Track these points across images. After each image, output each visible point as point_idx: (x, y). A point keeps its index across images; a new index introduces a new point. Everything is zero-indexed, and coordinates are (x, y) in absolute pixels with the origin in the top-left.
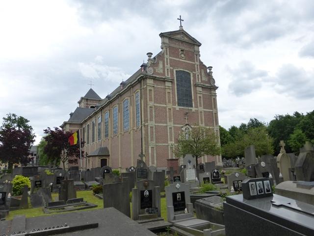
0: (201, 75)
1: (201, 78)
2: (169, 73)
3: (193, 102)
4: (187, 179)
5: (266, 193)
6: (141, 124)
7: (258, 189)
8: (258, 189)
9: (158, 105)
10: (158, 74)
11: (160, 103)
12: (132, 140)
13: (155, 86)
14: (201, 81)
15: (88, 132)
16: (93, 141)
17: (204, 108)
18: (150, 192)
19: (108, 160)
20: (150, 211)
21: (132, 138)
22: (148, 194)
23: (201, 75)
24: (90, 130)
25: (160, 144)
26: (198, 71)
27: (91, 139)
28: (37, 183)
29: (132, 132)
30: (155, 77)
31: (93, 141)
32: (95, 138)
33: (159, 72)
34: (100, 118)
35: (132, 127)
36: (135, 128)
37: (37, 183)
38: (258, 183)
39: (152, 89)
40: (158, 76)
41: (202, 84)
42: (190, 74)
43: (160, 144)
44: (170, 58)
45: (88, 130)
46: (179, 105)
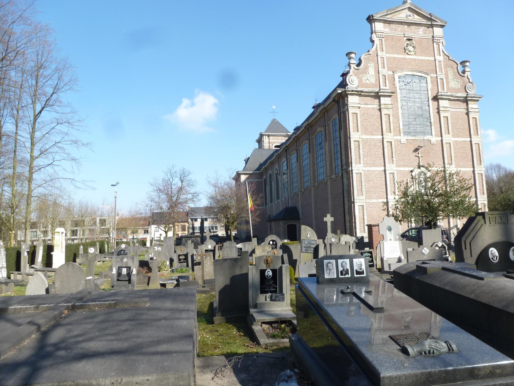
0: (447, 78)
1: (448, 84)
2: (387, 81)
4: (319, 257)
5: (355, 276)
6: (342, 170)
7: (340, 269)
8: (340, 269)
9: (369, 137)
10: (367, 86)
11: (372, 134)
12: (329, 195)
13: (362, 106)
14: (448, 89)
15: (271, 186)
16: (271, 201)
17: (454, 136)
18: (274, 271)
19: (297, 226)
20: (273, 298)
21: (329, 192)
22: (271, 274)
23: (447, 78)
24: (267, 187)
25: (373, 201)
26: (441, 70)
27: (274, 195)
28: (181, 257)
29: (329, 183)
30: (362, 92)
31: (271, 201)
32: (273, 198)
33: (368, 82)
34: (285, 163)
35: (328, 174)
36: (334, 176)
37: (181, 257)
38: (340, 261)
39: (357, 111)
40: (366, 90)
41: (449, 94)
42: (426, 78)
43: (373, 201)
44: (388, 55)
45: (271, 182)
46: (407, 133)
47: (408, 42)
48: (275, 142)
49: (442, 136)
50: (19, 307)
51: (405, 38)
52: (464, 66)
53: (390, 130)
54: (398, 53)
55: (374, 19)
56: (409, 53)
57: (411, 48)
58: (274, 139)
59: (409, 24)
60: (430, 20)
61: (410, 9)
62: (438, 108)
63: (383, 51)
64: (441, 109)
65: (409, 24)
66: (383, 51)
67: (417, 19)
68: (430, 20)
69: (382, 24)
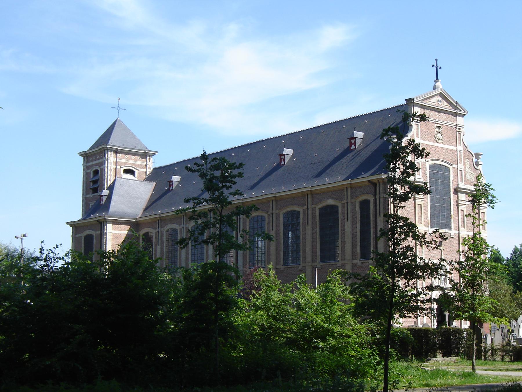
3: (452, 220)
26: (461, 163)
47: (438, 130)
48: (125, 164)
49: (459, 230)
50: (494, 264)
51: (436, 125)
52: (477, 158)
53: (421, 221)
54: (429, 140)
55: (413, 103)
56: (438, 141)
57: (439, 136)
58: (124, 158)
59: (440, 111)
60: (456, 108)
61: (441, 95)
62: (457, 201)
63: (464, 228)
64: (460, 202)
65: (440, 111)
66: (464, 228)
67: (444, 105)
68: (456, 108)
69: (419, 108)
